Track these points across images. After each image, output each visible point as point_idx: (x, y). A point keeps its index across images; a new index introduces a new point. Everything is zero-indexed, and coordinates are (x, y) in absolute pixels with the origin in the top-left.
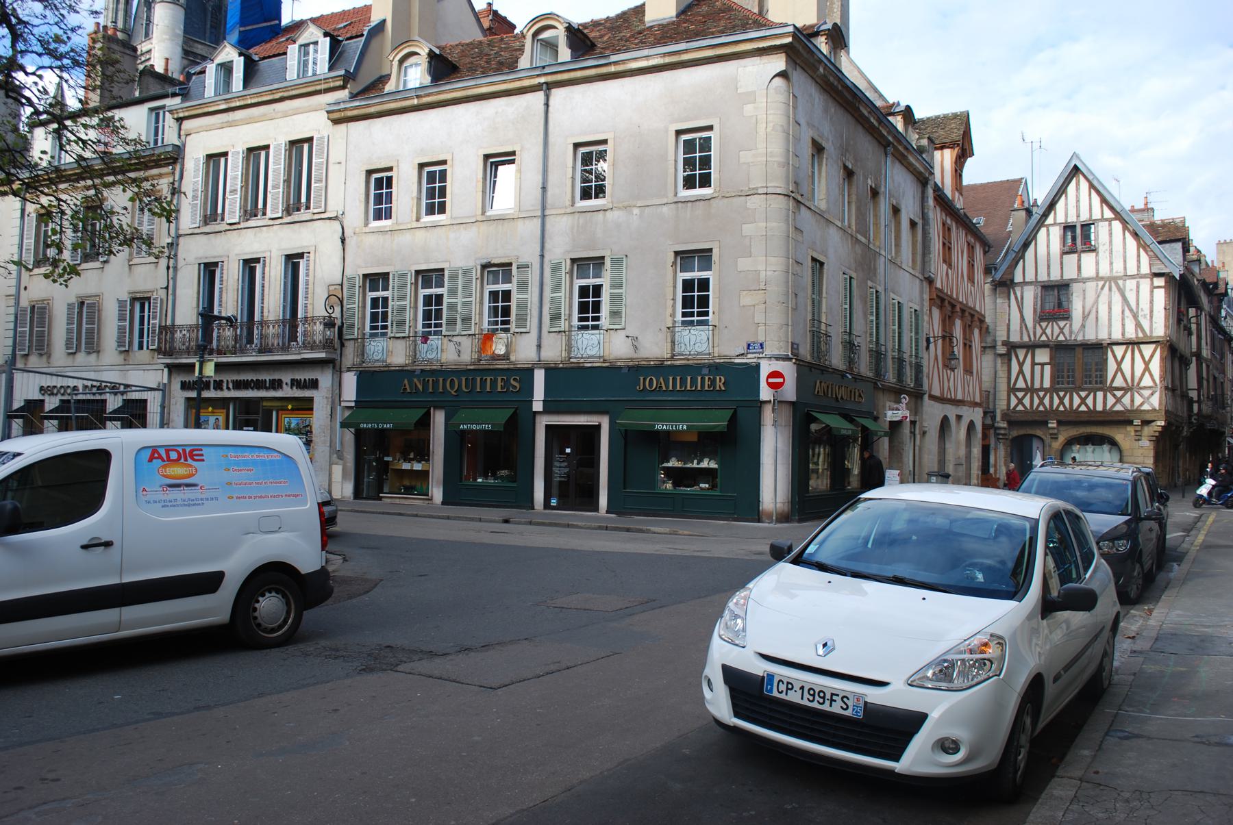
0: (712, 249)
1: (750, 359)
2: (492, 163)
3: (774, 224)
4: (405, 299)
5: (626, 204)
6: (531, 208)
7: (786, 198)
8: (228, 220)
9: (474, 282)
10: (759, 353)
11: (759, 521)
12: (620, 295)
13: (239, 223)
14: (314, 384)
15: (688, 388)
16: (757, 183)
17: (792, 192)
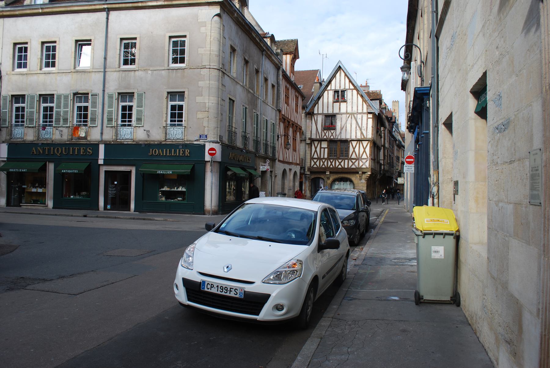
1: (201, 142)
5: (145, 68)
7: (218, 71)
10: (205, 140)
11: (204, 214)
12: (141, 111)
15: (173, 155)
16: (206, 63)
17: (221, 68)
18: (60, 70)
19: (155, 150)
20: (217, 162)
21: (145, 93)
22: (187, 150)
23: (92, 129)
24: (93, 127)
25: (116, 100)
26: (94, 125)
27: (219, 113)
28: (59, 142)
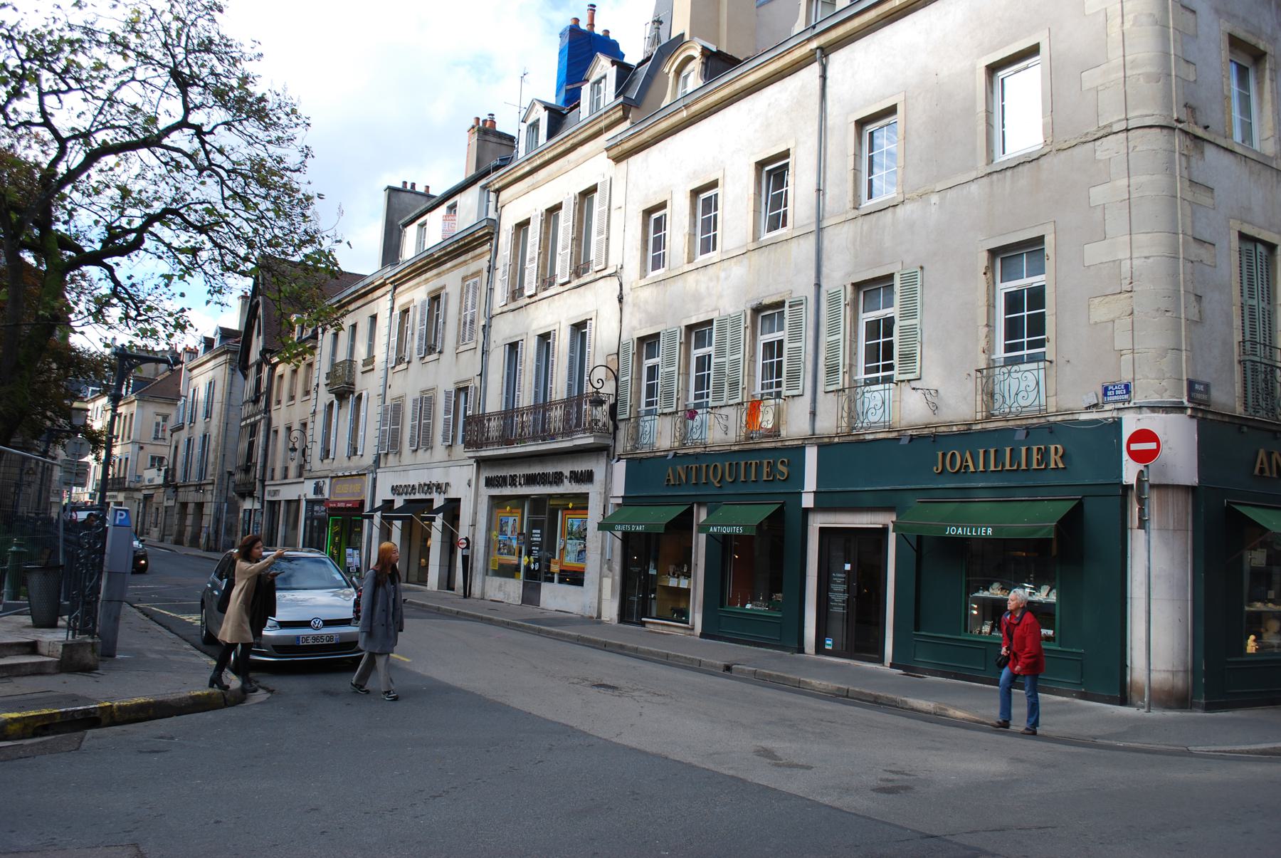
0: (1043, 237)
1: (1107, 414)
2: (769, 172)
3: (1144, 179)
4: (672, 364)
5: (921, 191)
6: (806, 222)
7: (1165, 132)
8: (560, 280)
9: (842, 309)
10: (1124, 402)
11: (1124, 701)
13: (569, 282)
14: (588, 477)
15: (1007, 467)
16: (1112, 116)
17: (1178, 121)
18: (727, 251)
19: (953, 454)
20: (1178, 486)
21: (922, 268)
22: (1056, 448)
23: (790, 401)
24: (793, 396)
25: (848, 308)
26: (795, 392)
27: (1182, 292)
28: (717, 449)
